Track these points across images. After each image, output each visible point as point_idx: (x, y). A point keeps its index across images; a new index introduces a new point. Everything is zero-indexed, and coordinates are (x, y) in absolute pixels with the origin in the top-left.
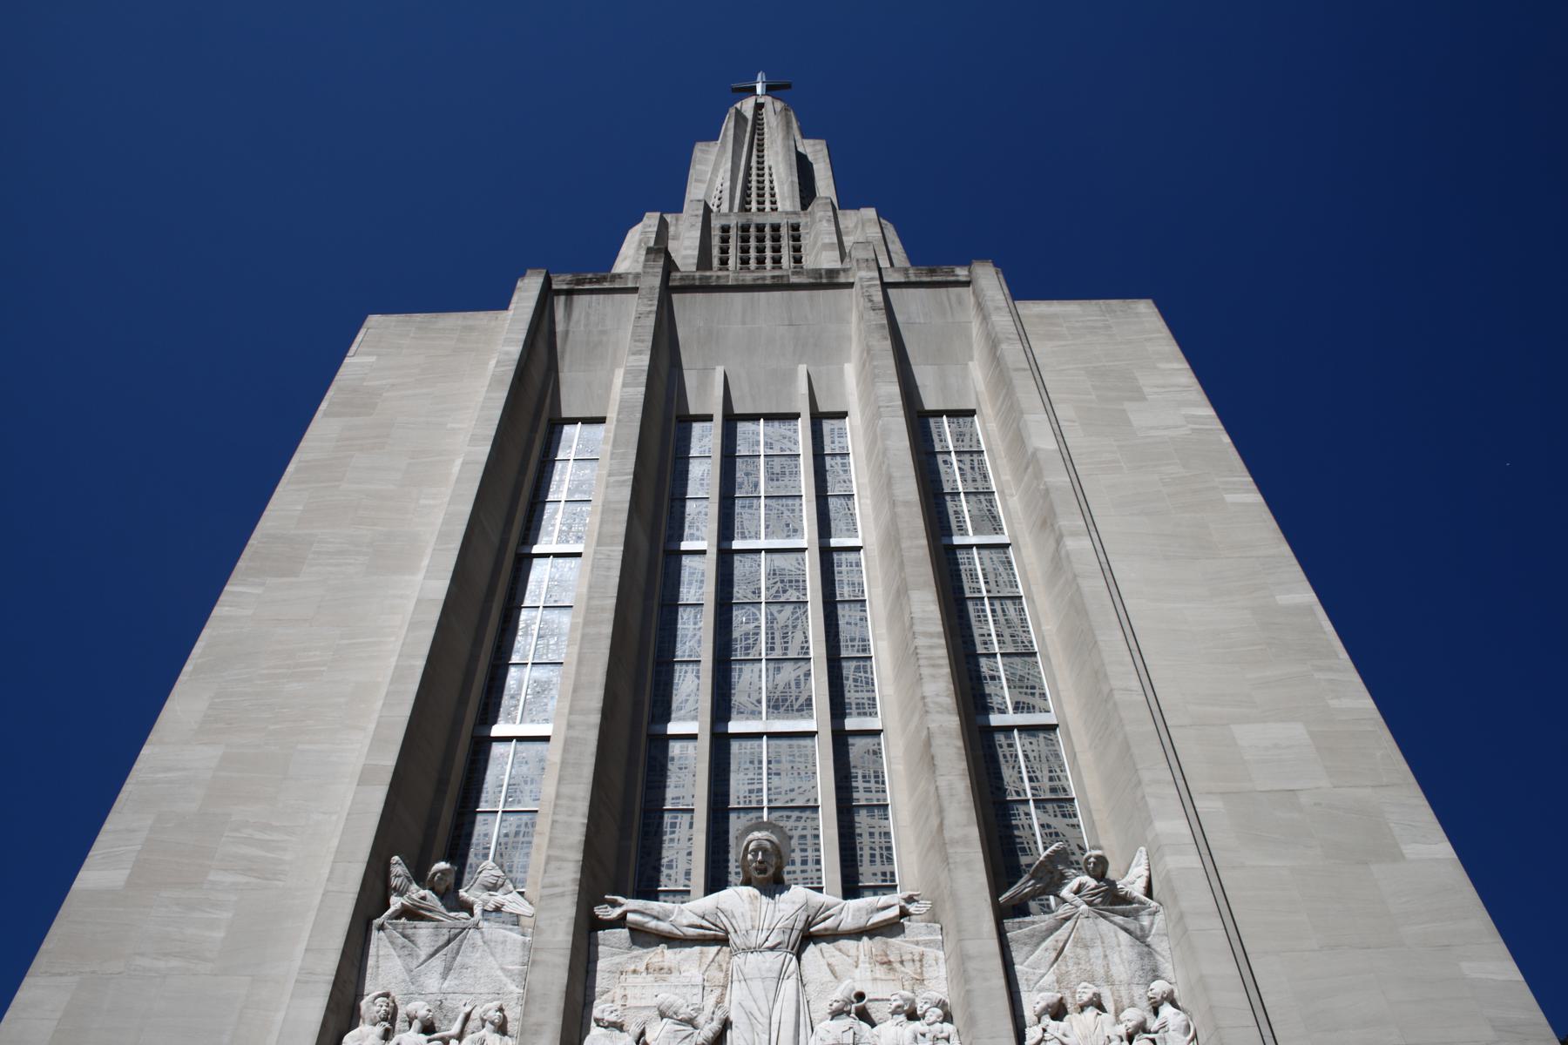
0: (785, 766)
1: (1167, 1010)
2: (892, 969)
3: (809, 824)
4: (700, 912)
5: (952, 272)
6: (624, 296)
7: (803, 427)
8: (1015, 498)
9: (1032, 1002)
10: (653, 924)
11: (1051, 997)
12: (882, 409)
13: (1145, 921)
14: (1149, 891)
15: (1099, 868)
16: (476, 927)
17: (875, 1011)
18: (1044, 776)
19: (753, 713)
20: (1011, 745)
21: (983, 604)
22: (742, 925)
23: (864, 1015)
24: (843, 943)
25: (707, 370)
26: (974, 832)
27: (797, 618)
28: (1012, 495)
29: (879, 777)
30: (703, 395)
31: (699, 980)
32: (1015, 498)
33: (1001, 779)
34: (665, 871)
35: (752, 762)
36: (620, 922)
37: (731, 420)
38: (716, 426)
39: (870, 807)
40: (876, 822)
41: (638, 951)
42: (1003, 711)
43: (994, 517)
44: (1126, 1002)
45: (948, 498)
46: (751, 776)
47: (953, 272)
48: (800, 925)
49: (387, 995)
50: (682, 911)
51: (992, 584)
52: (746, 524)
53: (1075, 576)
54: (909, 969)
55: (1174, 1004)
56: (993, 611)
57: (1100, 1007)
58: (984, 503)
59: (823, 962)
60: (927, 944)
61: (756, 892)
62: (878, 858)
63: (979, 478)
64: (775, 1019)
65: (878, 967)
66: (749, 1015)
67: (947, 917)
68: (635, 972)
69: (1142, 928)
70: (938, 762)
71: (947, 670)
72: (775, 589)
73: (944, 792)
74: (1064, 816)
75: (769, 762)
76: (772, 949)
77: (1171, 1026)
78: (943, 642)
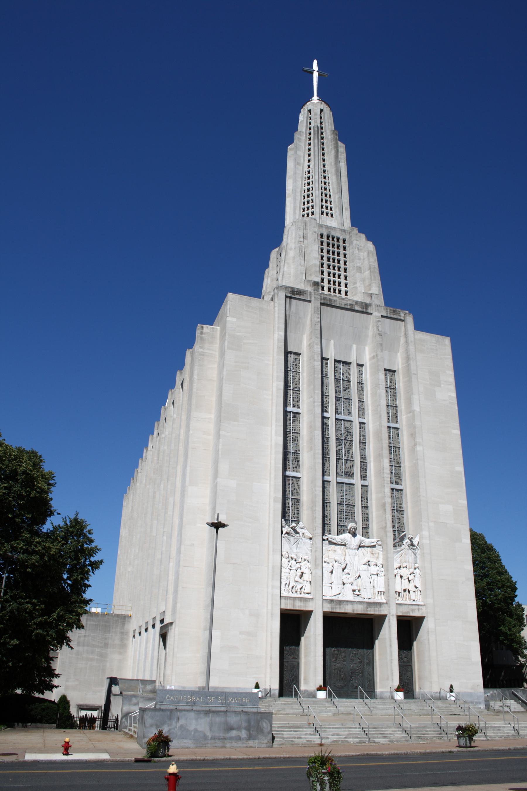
2: (373, 555)
3: (353, 509)
5: (399, 314)
10: (333, 541)
13: (417, 552)
18: (399, 503)
19: (341, 475)
22: (349, 543)
24: (365, 548)
25: (328, 340)
32: (404, 417)
40: (366, 510)
41: (330, 546)
47: (400, 313)
48: (359, 544)
53: (417, 459)
54: (376, 555)
56: (393, 451)
57: (406, 567)
60: (380, 550)
61: (351, 536)
63: (394, 399)
66: (350, 562)
73: (387, 519)
77: (417, 573)
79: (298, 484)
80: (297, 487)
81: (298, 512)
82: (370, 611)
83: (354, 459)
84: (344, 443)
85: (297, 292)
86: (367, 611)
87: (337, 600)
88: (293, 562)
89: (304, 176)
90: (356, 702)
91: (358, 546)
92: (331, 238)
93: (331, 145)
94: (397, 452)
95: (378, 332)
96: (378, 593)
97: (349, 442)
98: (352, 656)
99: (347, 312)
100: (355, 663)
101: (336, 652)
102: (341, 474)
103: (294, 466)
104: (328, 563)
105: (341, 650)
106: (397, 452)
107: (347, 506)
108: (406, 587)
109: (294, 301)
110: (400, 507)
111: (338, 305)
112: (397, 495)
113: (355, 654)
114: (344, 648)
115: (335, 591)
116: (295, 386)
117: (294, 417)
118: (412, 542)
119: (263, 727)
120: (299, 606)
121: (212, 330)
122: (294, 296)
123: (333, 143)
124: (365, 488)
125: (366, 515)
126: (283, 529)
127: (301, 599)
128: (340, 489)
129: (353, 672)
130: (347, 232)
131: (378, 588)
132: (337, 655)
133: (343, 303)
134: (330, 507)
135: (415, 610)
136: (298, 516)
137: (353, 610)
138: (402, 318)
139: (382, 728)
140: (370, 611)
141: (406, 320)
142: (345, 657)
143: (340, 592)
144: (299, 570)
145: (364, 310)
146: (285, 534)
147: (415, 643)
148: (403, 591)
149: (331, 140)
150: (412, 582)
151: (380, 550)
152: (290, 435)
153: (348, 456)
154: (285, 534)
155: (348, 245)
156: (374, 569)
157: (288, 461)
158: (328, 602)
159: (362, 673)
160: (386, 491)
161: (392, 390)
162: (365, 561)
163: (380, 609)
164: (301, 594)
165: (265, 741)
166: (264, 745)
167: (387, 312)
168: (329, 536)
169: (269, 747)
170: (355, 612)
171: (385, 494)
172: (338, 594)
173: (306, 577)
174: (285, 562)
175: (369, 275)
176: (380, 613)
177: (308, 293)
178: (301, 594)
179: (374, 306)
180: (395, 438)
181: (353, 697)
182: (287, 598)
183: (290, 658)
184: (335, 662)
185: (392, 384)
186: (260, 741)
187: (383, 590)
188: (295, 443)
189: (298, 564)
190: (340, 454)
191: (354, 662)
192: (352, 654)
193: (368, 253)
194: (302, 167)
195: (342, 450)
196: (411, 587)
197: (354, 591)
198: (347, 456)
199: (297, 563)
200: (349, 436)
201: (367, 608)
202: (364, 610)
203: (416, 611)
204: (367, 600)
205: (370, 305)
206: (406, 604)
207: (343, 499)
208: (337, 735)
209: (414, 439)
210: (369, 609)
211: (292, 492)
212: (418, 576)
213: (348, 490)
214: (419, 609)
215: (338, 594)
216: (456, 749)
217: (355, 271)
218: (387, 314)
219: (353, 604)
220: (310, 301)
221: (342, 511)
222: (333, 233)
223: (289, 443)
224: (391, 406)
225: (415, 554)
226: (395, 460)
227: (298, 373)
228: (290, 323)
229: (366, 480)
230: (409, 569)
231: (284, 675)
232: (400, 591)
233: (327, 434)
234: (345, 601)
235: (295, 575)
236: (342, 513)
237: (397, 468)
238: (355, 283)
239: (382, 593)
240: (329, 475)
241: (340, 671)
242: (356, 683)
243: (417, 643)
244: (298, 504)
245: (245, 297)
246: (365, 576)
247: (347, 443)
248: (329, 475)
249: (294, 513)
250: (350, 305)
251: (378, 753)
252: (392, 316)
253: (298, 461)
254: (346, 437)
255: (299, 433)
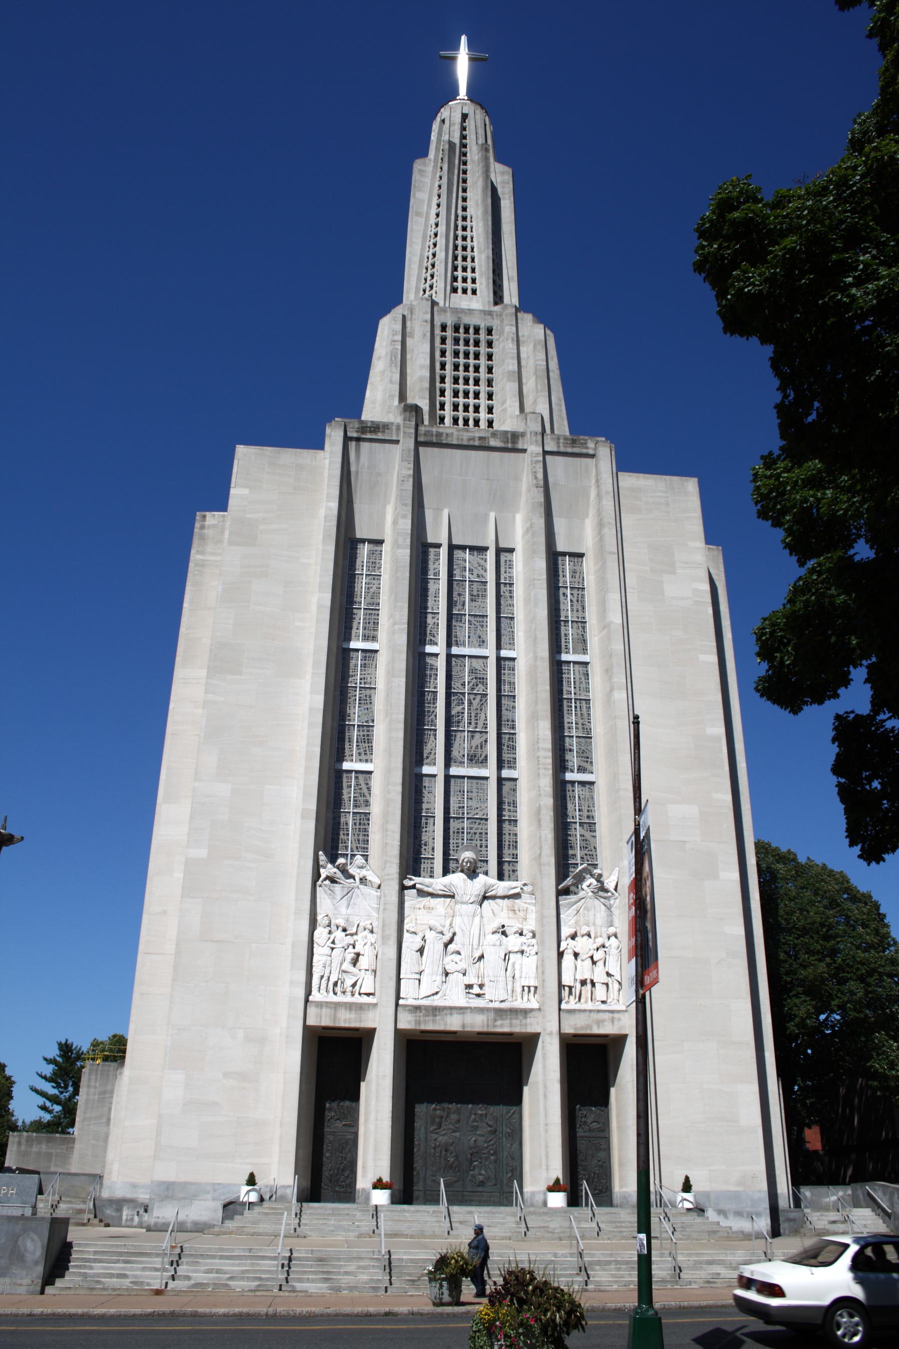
0: (474, 794)
1: (613, 939)
2: (515, 913)
3: (484, 827)
4: (444, 884)
5: (584, 445)
6: (391, 445)
7: (491, 555)
8: (597, 638)
9: (566, 931)
10: (426, 889)
11: (572, 931)
12: (536, 582)
13: (612, 902)
14: (616, 889)
15: (599, 878)
16: (358, 888)
17: (508, 930)
18: (585, 808)
19: (461, 763)
20: (573, 791)
21: (571, 703)
23: (504, 933)
24: (498, 900)
25: (438, 510)
26: (552, 860)
27: (482, 704)
28: (595, 636)
29: (514, 804)
30: (437, 533)
31: (443, 914)
32: (597, 638)
33: (567, 809)
34: (424, 847)
35: (460, 791)
36: (414, 887)
37: (452, 548)
38: (444, 552)
39: (510, 821)
40: (512, 828)
41: (421, 899)
42: (572, 771)
43: (584, 640)
44: (599, 934)
45: (562, 623)
46: (459, 799)
47: (586, 443)
48: (482, 893)
49: (327, 916)
50: (437, 883)
51: (578, 688)
52: (458, 634)
54: (521, 914)
55: (616, 937)
56: (576, 707)
58: (581, 628)
59: (490, 909)
60: (529, 904)
61: (466, 877)
62: (511, 847)
63: (580, 608)
64: (472, 933)
65: (510, 912)
66: (463, 930)
67: (538, 894)
68: (419, 909)
69: (610, 904)
70: (542, 823)
71: (550, 772)
72: (472, 683)
73: (543, 838)
74: (591, 831)
75: (468, 792)
76: (471, 903)
78: (550, 754)
79: (367, 784)
80: (365, 791)
81: (366, 838)
82: (502, 1026)
83: (488, 730)
84: (469, 700)
85: (370, 427)
86: (495, 1026)
87: (429, 1006)
88: (339, 934)
89: (429, 233)
90: (428, 1212)
91: (480, 897)
92: (462, 330)
93: (478, 171)
94: (584, 709)
95: (535, 482)
96: (523, 990)
97: (479, 697)
98: (475, 1121)
99: (473, 453)
100: (478, 1135)
101: (438, 1112)
102: (460, 759)
103: (362, 751)
104: (415, 933)
105: (450, 1109)
106: (584, 709)
107: (470, 821)
108: (587, 976)
109: (365, 446)
110: (588, 817)
111: (455, 442)
112: (581, 793)
113: (481, 1115)
114: (457, 1103)
115: (425, 990)
116: (369, 600)
117: (364, 658)
118: (602, 883)
119: (26, 1250)
120: (345, 1021)
121: (221, 519)
122: (364, 436)
123: (481, 165)
124: (512, 783)
125: (511, 837)
126: (322, 870)
127: (350, 1006)
128: (458, 789)
129: (476, 1153)
130: (495, 314)
131: (523, 980)
132: (441, 1117)
133: (465, 438)
134: (434, 825)
135: (603, 1021)
136: (366, 846)
137: (463, 1026)
138: (591, 452)
139: (339, 1259)
140: (502, 1026)
141: (597, 455)
142: (458, 1121)
143: (438, 990)
144: (351, 949)
145: (510, 446)
146: (325, 879)
147: (613, 1091)
148: (578, 985)
149: (478, 162)
150: (600, 964)
151: (529, 904)
152: (355, 693)
153: (477, 724)
154: (325, 879)
155: (497, 337)
156: (514, 942)
157: (349, 741)
158: (409, 1010)
159: (495, 1154)
160: (542, 785)
161: (575, 592)
162: (495, 925)
163: (524, 1021)
164: (353, 995)
165: (27, 1281)
166: (22, 1290)
167: (558, 443)
168: (417, 880)
169: (32, 1293)
170: (468, 1029)
171: (539, 790)
172: (433, 995)
173: (363, 962)
174: (321, 934)
175: (534, 384)
176: (524, 1030)
177: (394, 428)
178: (353, 995)
179: (529, 435)
180: (581, 683)
181: (474, 1203)
182: (320, 1005)
183: (339, 1124)
184: (437, 1133)
185: (577, 579)
186: (14, 1281)
187: (533, 983)
188: (366, 707)
189: (349, 937)
190: (458, 722)
191: (478, 1133)
192: (473, 1116)
193: (535, 347)
194: (424, 219)
195: (463, 713)
196: (599, 975)
197: (469, 987)
198: (473, 725)
199: (346, 935)
200: (480, 685)
201: (495, 1020)
202: (488, 1025)
203: (605, 1023)
204: (497, 1005)
205: (523, 435)
206: (584, 1011)
207: (463, 807)
208: (217, 1273)
209: (610, 678)
210: (499, 1023)
211: (355, 801)
212: (614, 952)
213: (474, 790)
214: (613, 1020)
215: (433, 995)
216: (429, 1308)
217: (505, 380)
218: (559, 447)
219: (463, 1013)
220: (397, 442)
221: (461, 831)
222: (466, 320)
223: (352, 708)
224: (572, 621)
225: (609, 908)
226: (580, 726)
227: (376, 577)
228: (358, 489)
229: (514, 768)
230: (596, 937)
231: (324, 1159)
232: (572, 984)
233: (432, 686)
234: (445, 1008)
235: (341, 958)
236: (460, 835)
237: (583, 740)
238: (504, 402)
239: (532, 989)
240: (435, 764)
241: (446, 1151)
242: (480, 1174)
243: (617, 1091)
244: (366, 822)
245: (268, 450)
246: (494, 956)
247: (474, 699)
248: (435, 764)
249: (359, 840)
250: (480, 438)
251: (200, 1310)
252: (569, 450)
253: (370, 741)
254: (473, 689)
255: (375, 688)
